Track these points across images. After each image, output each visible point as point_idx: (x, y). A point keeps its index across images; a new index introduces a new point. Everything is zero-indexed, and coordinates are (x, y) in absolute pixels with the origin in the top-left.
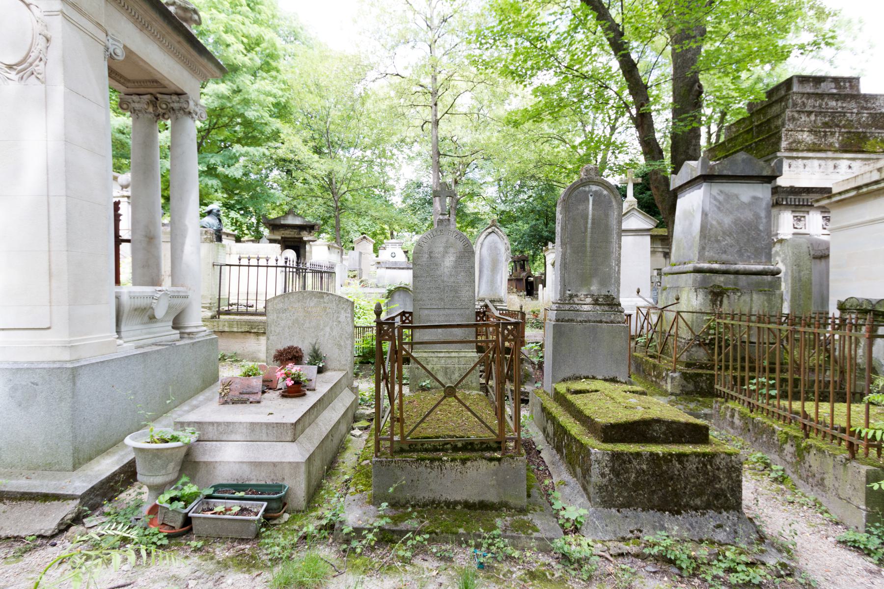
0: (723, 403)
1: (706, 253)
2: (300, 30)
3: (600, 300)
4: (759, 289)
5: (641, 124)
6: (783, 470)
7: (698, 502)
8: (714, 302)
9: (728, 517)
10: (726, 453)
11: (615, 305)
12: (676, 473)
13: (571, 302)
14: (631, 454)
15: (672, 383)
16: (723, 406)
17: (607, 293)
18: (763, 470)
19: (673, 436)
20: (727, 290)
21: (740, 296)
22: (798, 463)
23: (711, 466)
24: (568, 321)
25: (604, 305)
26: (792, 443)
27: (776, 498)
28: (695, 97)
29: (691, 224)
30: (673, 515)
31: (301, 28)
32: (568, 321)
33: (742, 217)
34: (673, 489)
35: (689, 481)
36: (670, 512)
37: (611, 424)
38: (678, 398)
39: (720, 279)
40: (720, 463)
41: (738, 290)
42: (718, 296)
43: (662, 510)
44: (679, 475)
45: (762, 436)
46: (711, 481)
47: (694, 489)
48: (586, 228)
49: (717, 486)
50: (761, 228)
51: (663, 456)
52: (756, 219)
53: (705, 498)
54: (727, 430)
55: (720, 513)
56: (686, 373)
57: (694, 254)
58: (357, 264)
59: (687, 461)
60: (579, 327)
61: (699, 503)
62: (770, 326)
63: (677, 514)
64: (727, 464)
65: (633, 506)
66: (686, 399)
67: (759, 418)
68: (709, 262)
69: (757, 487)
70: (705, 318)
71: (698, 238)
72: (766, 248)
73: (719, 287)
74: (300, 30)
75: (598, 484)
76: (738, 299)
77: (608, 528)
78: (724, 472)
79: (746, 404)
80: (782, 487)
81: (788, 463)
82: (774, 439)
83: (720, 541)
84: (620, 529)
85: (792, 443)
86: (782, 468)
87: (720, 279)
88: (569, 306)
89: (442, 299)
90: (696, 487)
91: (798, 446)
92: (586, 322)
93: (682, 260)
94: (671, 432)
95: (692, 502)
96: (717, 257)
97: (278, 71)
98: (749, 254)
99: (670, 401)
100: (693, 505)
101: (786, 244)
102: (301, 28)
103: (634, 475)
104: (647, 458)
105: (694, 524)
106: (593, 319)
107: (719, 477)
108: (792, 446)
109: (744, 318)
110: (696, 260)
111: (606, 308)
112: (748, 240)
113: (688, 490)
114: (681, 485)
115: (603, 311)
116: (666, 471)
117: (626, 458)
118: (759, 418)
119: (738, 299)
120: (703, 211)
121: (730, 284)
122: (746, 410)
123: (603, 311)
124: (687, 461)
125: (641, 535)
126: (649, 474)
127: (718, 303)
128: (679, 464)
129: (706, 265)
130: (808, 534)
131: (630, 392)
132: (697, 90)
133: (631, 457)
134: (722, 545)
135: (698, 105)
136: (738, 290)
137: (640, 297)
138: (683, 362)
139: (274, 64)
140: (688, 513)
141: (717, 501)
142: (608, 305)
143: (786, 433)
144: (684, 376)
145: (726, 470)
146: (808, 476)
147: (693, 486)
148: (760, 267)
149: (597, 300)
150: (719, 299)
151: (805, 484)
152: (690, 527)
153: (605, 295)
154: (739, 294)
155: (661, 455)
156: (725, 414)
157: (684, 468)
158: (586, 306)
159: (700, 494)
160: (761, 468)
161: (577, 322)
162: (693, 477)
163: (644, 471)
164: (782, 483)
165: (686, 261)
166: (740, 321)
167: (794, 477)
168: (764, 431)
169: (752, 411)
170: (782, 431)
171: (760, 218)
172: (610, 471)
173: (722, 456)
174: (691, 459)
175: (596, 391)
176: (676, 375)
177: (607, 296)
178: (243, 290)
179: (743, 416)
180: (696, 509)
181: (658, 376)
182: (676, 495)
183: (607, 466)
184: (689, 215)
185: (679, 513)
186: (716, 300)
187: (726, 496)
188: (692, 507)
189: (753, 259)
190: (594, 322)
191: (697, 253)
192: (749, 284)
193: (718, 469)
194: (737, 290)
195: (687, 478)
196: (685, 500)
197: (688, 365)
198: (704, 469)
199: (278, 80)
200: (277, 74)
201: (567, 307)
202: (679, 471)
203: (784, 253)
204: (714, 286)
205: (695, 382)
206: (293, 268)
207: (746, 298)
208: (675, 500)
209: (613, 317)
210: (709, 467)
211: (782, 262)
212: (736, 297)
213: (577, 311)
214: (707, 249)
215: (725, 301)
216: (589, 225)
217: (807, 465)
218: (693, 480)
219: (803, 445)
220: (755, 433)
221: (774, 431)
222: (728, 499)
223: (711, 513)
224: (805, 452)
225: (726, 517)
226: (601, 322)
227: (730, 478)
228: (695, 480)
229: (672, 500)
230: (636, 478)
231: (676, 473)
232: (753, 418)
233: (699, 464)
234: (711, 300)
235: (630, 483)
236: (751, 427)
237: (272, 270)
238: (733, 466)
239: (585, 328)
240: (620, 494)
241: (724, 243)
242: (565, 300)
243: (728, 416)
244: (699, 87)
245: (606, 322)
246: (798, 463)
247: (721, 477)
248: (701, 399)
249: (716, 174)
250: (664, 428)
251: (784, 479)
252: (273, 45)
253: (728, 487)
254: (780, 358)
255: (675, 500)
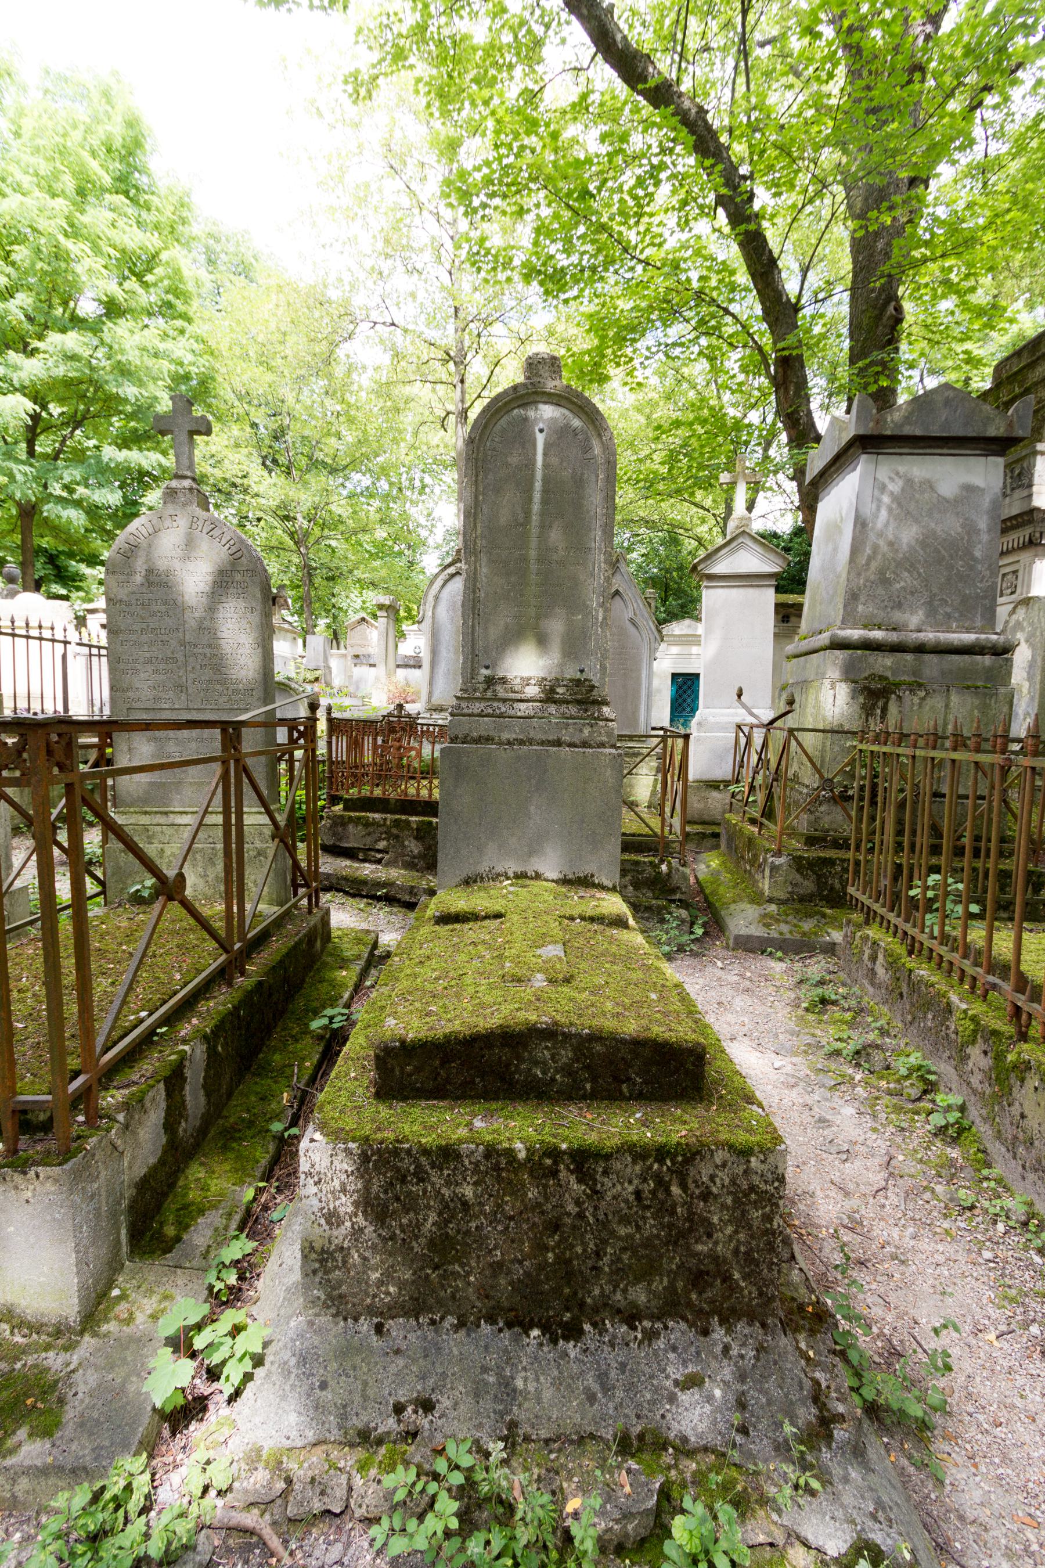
0: (859, 927)
1: (860, 608)
2: (253, 261)
3: (560, 690)
4: (966, 684)
5: (784, 383)
6: (962, 1109)
7: (639, 1295)
8: (868, 711)
9: (726, 1349)
10: (731, 1147)
11: (595, 702)
12: (571, 1208)
13: (489, 694)
14: (426, 1151)
15: (771, 877)
16: (859, 934)
17: (578, 675)
18: (919, 1099)
19: (594, 1080)
20: (897, 685)
21: (923, 699)
22: (997, 1098)
23: (684, 1186)
24: (478, 740)
25: (568, 702)
26: (985, 1047)
27: (933, 1191)
28: (887, 330)
29: (835, 550)
30: (554, 1341)
31: (255, 257)
32: (478, 740)
33: (938, 530)
34: (558, 1258)
35: (613, 1233)
36: (545, 1329)
37: (403, 1042)
38: (783, 908)
39: (884, 663)
40: (712, 1178)
41: (920, 685)
42: (878, 698)
43: (521, 1324)
44: (581, 1216)
45: (925, 1013)
46: (683, 1234)
47: (625, 1257)
48: (528, 513)
49: (700, 1247)
50: (978, 554)
51: (528, 1159)
52: (968, 533)
53: (660, 1284)
54: (862, 987)
55: (706, 1332)
56: (801, 858)
57: (837, 612)
58: (321, 659)
59: (606, 1173)
60: (504, 755)
61: (643, 1298)
62: (982, 758)
63: (566, 1339)
64: (733, 1182)
65: (430, 1310)
66: (797, 911)
67: (923, 972)
68: (865, 627)
69: (892, 1151)
70: (848, 744)
71: (844, 576)
72: (985, 597)
73: (882, 678)
74: (253, 261)
75: (317, 1246)
76: (920, 705)
77: (327, 1395)
78: (724, 1206)
79: (900, 934)
80: (954, 1153)
81: (974, 1091)
82: (948, 1028)
83: (685, 1440)
84: (365, 1398)
85: (985, 1047)
86: (960, 1101)
87: (884, 663)
88: (482, 705)
89: (180, 688)
90: (635, 1253)
91: (999, 1057)
92: (521, 742)
93: (817, 626)
94: (587, 1067)
95: (618, 1296)
96: (880, 615)
97: (189, 320)
98: (949, 610)
99: (766, 915)
100: (623, 1304)
101: (1036, 607)
102: (255, 257)
103: (433, 1217)
104: (477, 1164)
105: (613, 1374)
106: (539, 736)
107: (706, 1222)
108: (985, 1053)
109: (921, 742)
110: (839, 623)
111: (573, 710)
112: (949, 580)
113: (606, 1260)
114: (584, 1245)
115: (564, 716)
116: (539, 1205)
117: (406, 1164)
118: (923, 972)
119: (920, 705)
120: (857, 517)
121: (904, 673)
122: (901, 950)
123: (564, 716)
124: (606, 1173)
125: (424, 1422)
126: (482, 1212)
127: (879, 711)
128: (580, 1181)
129: (855, 634)
130: (992, 1337)
131: (583, 918)
132: (892, 316)
133: (423, 1160)
134: (690, 1454)
135: (892, 341)
136: (920, 685)
137: (744, 706)
138: (802, 834)
139: (180, 306)
140: (601, 1332)
141: (700, 1294)
142: (578, 702)
143: (974, 1019)
144: (799, 864)
145: (729, 1201)
146: (1015, 1137)
147: (624, 1249)
148: (969, 638)
149: (552, 690)
150: (880, 704)
151: (1009, 1156)
152: (595, 1387)
153: (571, 680)
154: (923, 694)
155: (522, 1155)
156: (862, 952)
157: (596, 1194)
158: (523, 706)
159: (646, 1273)
160: (914, 1093)
161: (501, 743)
162: (625, 1220)
163: (465, 1204)
164: (955, 1141)
165: (823, 627)
166: (934, 748)
167: (983, 1129)
168: (929, 1003)
169: (910, 953)
170: (965, 1011)
171: (978, 532)
172: (356, 1204)
173: (719, 1156)
174: (617, 1165)
175: (498, 916)
176: (782, 860)
177: (578, 682)
178: (22, 692)
179: (893, 964)
180: (631, 1317)
181: (753, 862)
182: (570, 1276)
183: (344, 1190)
184: (835, 528)
185: (573, 1332)
186: (873, 706)
187: (727, 1278)
188: (619, 1311)
189: (957, 620)
190: (542, 743)
191: (841, 606)
192: (943, 673)
193: (706, 1196)
194: (916, 686)
195: (604, 1224)
196: (597, 1291)
197: (811, 841)
198: (661, 1195)
199: (187, 336)
200: (185, 324)
201: (478, 707)
202: (578, 1203)
203: (1031, 624)
204: (872, 677)
205: (819, 877)
206: (99, 648)
207: (936, 702)
208: (567, 1291)
209: (587, 731)
210: (675, 1190)
211: (1027, 641)
212: (916, 700)
213: (501, 716)
214: (862, 599)
215: (893, 708)
216: (536, 507)
217: (1016, 1110)
218: (623, 1231)
219: (1011, 1057)
220: (912, 1005)
221: (949, 1009)
222: (732, 1288)
223: (678, 1330)
224: (1013, 1075)
225: (718, 1349)
226: (558, 743)
227: (741, 1222)
228: (630, 1230)
229: (557, 1290)
230: (442, 1224)
231: (571, 1208)
232: (910, 971)
233: (645, 1180)
234: (863, 707)
235: (423, 1241)
236: (905, 989)
237: (21, 642)
238: (752, 1188)
239: (518, 758)
240: (388, 1275)
241: (898, 586)
242: (475, 690)
243: (866, 956)
244: (896, 309)
245: (571, 745)
246: (997, 1098)
247: (715, 1219)
248: (829, 911)
249: (888, 433)
250: (566, 1055)
251: (961, 1131)
252: (177, 271)
253: (736, 1252)
254: (999, 827)
255: (567, 1291)
